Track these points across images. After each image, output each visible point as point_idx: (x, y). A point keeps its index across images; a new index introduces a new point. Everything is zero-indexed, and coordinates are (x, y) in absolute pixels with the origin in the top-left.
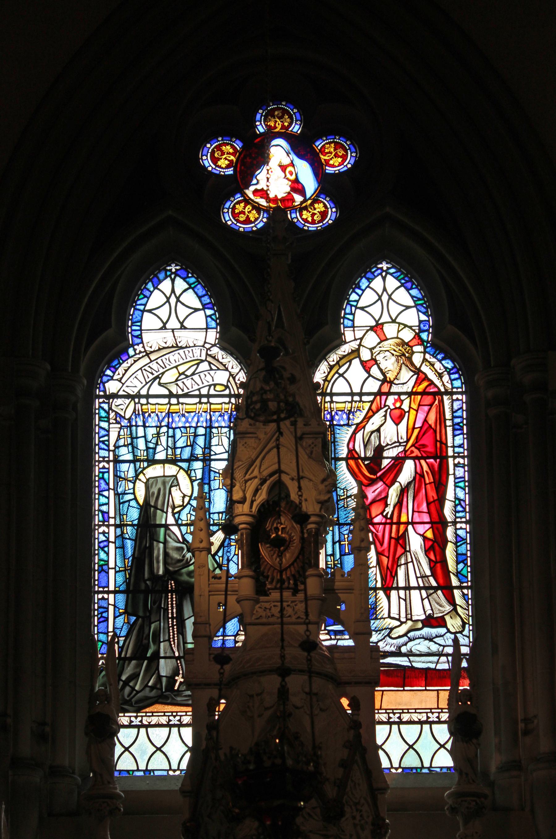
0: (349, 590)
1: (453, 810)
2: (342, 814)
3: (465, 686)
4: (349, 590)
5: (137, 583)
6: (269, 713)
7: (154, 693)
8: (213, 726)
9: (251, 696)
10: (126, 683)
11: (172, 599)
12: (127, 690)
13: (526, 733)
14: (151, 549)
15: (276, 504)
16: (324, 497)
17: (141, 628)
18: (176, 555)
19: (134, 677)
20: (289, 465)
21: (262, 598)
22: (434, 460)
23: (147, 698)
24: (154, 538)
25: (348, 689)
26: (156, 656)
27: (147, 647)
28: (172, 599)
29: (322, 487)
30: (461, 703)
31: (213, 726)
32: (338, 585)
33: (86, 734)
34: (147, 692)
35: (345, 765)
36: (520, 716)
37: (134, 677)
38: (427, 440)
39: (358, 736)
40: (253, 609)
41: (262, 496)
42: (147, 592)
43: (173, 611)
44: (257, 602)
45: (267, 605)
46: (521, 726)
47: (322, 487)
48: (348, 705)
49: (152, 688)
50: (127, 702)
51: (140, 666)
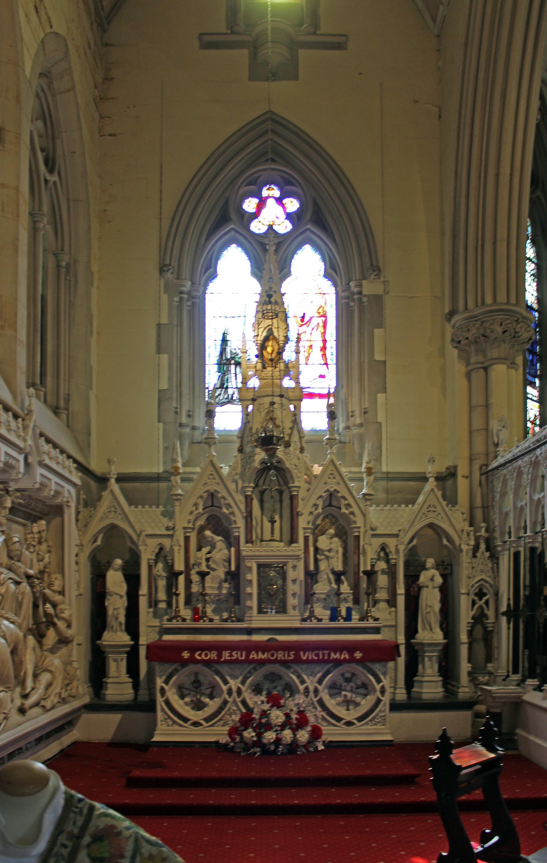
0: (294, 367)
1: (327, 444)
2: (290, 446)
3: (332, 400)
4: (294, 367)
5: (221, 361)
6: (266, 410)
7: (227, 400)
8: (247, 415)
9: (260, 404)
10: (217, 397)
11: (233, 367)
12: (217, 399)
13: (352, 416)
14: (225, 349)
15: (269, 336)
16: (286, 335)
17: (222, 378)
18: (234, 351)
19: (220, 395)
20: (275, 325)
21: (265, 370)
22: (506, 611)
23: (224, 402)
24: (226, 345)
25: (293, 402)
26: (227, 388)
27: (224, 384)
28: (233, 367)
29: (285, 331)
30: (494, 722)
31: (247, 415)
32: (290, 365)
33: (206, 417)
34: (224, 400)
35: (292, 429)
36: (350, 410)
37: (220, 395)
38: (321, 310)
39: (296, 419)
40: (261, 374)
41: (265, 334)
42: (224, 364)
43: (233, 371)
44: (262, 371)
45: (266, 372)
46: (350, 414)
47: (285, 331)
48: (399, 656)
49: (226, 398)
50: (218, 403)
51: (222, 391)
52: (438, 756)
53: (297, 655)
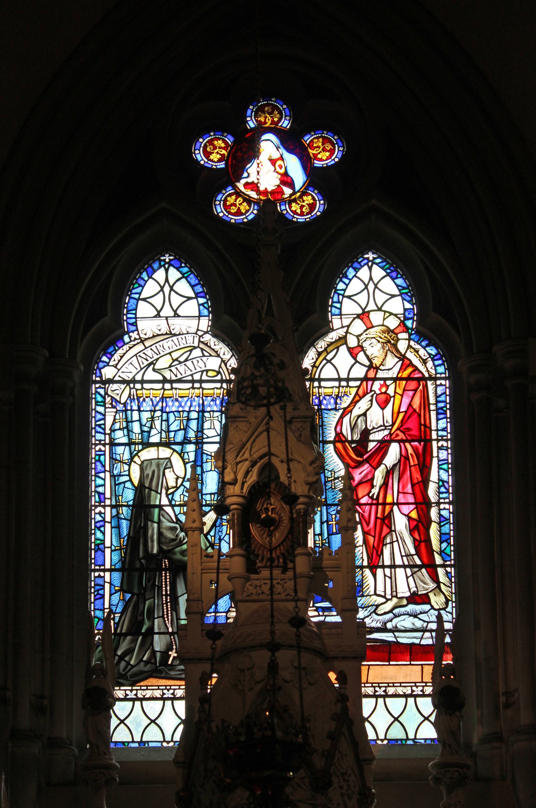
0: (337, 568)
1: (437, 780)
2: (330, 784)
3: (448, 660)
4: (337, 568)
5: (132, 562)
6: (259, 687)
7: (148, 667)
8: (205, 700)
9: (242, 671)
10: (122, 658)
11: (166, 577)
12: (123, 664)
13: (507, 706)
14: (145, 529)
15: (267, 485)
16: (312, 479)
17: (136, 605)
18: (169, 535)
19: (129, 652)
20: (278, 448)
21: (253, 576)
23: (141, 672)
24: (149, 518)
25: (336, 663)
26: (151, 632)
27: (142, 623)
28: (166, 577)
29: (310, 469)
31: (205, 700)
32: (326, 563)
33: (83, 707)
34: (141, 667)
35: (333, 736)
36: (501, 690)
37: (129, 652)
38: (412, 424)
39: (345, 709)
40: (244, 587)
41: (253, 478)
42: (142, 570)
43: (166, 589)
44: (248, 579)
45: (258, 583)
46: (502, 699)
47: (310, 469)
49: (147, 663)
50: (122, 676)
51: (135, 641)
52: (413, 298)
53: (158, 688)
